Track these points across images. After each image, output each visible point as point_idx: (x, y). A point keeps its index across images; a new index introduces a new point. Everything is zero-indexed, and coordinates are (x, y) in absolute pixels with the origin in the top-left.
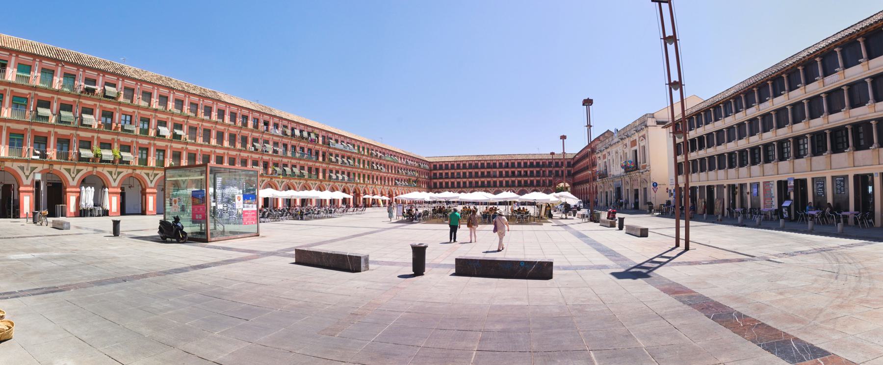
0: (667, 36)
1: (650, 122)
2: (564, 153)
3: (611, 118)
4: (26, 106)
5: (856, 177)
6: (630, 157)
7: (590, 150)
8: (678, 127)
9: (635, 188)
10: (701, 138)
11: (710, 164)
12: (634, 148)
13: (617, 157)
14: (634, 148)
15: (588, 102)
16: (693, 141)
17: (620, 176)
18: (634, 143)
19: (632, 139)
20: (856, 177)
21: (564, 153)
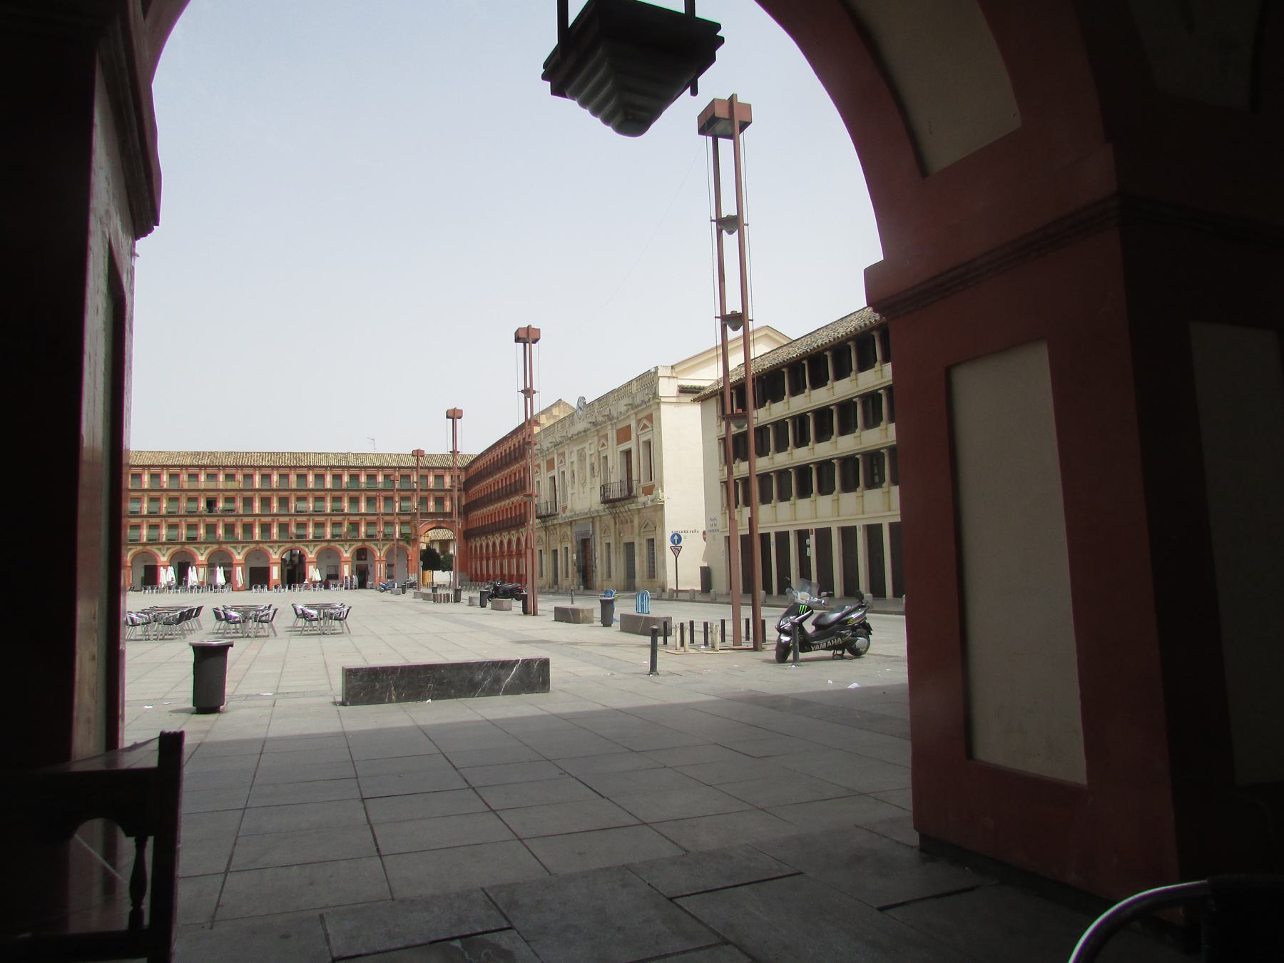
0: (724, 215)
1: (667, 388)
2: (454, 452)
3: (577, 375)
4: (394, 502)
5: (777, 533)
6: (616, 476)
7: (513, 452)
8: (732, 399)
9: (627, 539)
10: (780, 426)
11: (805, 481)
12: (625, 446)
13: (582, 468)
14: (625, 446)
15: (526, 337)
16: (761, 431)
17: (593, 518)
18: (624, 435)
19: (620, 426)
20: (777, 533)
21: (454, 452)
